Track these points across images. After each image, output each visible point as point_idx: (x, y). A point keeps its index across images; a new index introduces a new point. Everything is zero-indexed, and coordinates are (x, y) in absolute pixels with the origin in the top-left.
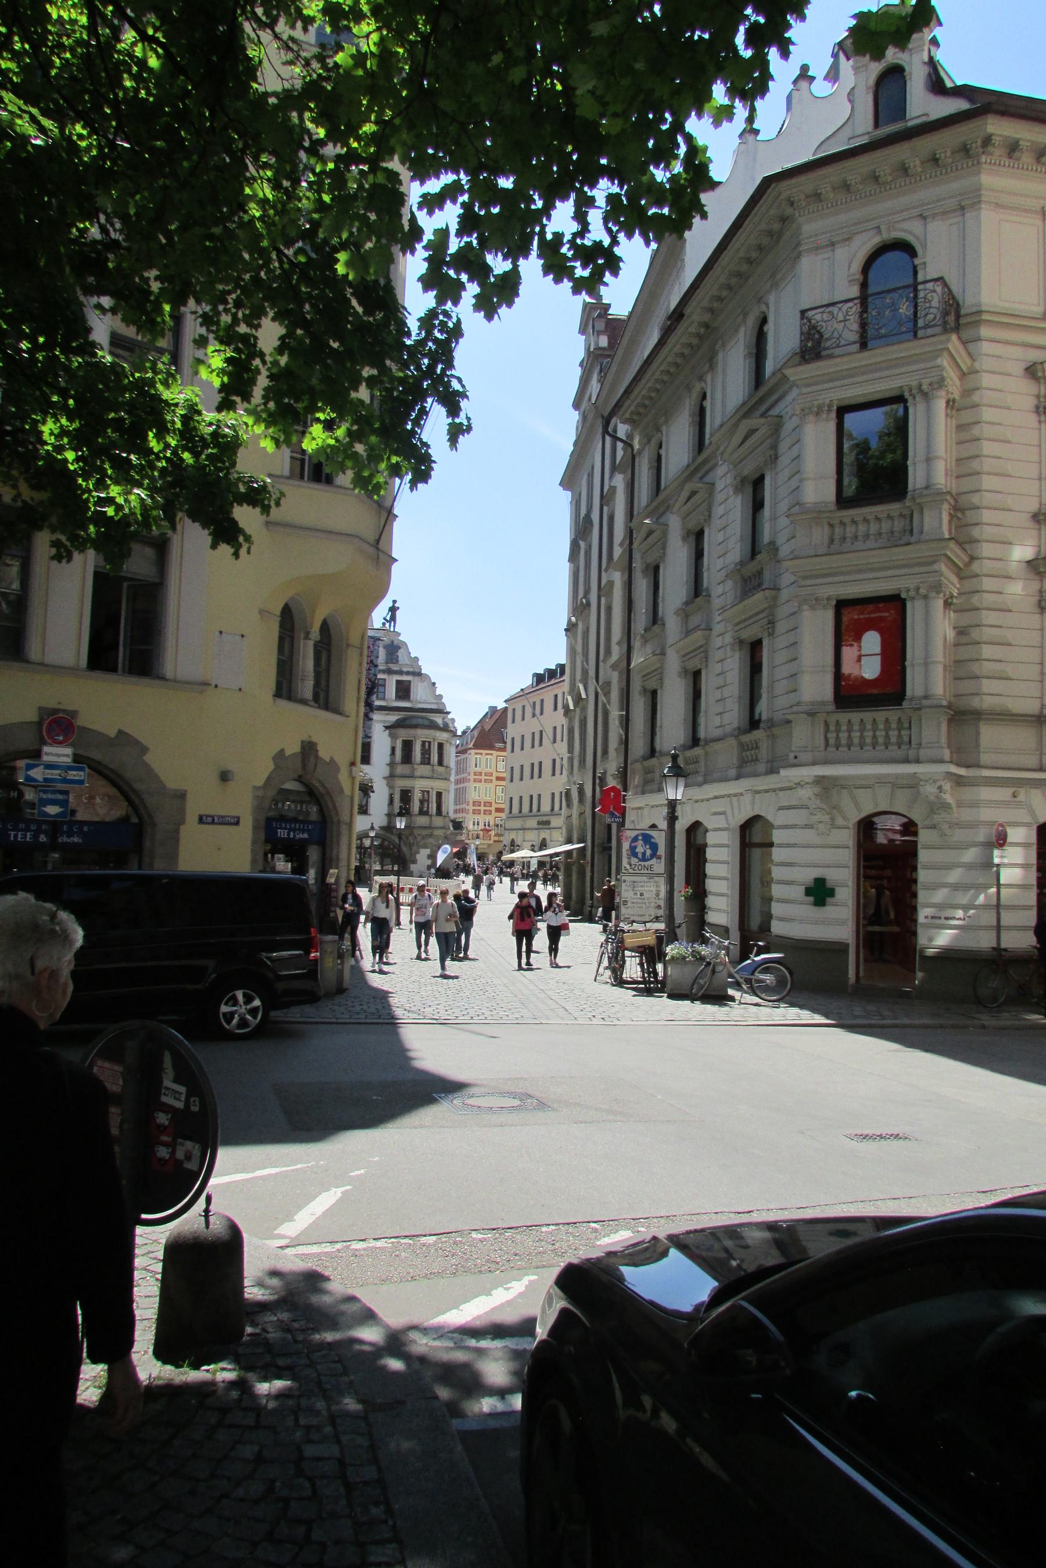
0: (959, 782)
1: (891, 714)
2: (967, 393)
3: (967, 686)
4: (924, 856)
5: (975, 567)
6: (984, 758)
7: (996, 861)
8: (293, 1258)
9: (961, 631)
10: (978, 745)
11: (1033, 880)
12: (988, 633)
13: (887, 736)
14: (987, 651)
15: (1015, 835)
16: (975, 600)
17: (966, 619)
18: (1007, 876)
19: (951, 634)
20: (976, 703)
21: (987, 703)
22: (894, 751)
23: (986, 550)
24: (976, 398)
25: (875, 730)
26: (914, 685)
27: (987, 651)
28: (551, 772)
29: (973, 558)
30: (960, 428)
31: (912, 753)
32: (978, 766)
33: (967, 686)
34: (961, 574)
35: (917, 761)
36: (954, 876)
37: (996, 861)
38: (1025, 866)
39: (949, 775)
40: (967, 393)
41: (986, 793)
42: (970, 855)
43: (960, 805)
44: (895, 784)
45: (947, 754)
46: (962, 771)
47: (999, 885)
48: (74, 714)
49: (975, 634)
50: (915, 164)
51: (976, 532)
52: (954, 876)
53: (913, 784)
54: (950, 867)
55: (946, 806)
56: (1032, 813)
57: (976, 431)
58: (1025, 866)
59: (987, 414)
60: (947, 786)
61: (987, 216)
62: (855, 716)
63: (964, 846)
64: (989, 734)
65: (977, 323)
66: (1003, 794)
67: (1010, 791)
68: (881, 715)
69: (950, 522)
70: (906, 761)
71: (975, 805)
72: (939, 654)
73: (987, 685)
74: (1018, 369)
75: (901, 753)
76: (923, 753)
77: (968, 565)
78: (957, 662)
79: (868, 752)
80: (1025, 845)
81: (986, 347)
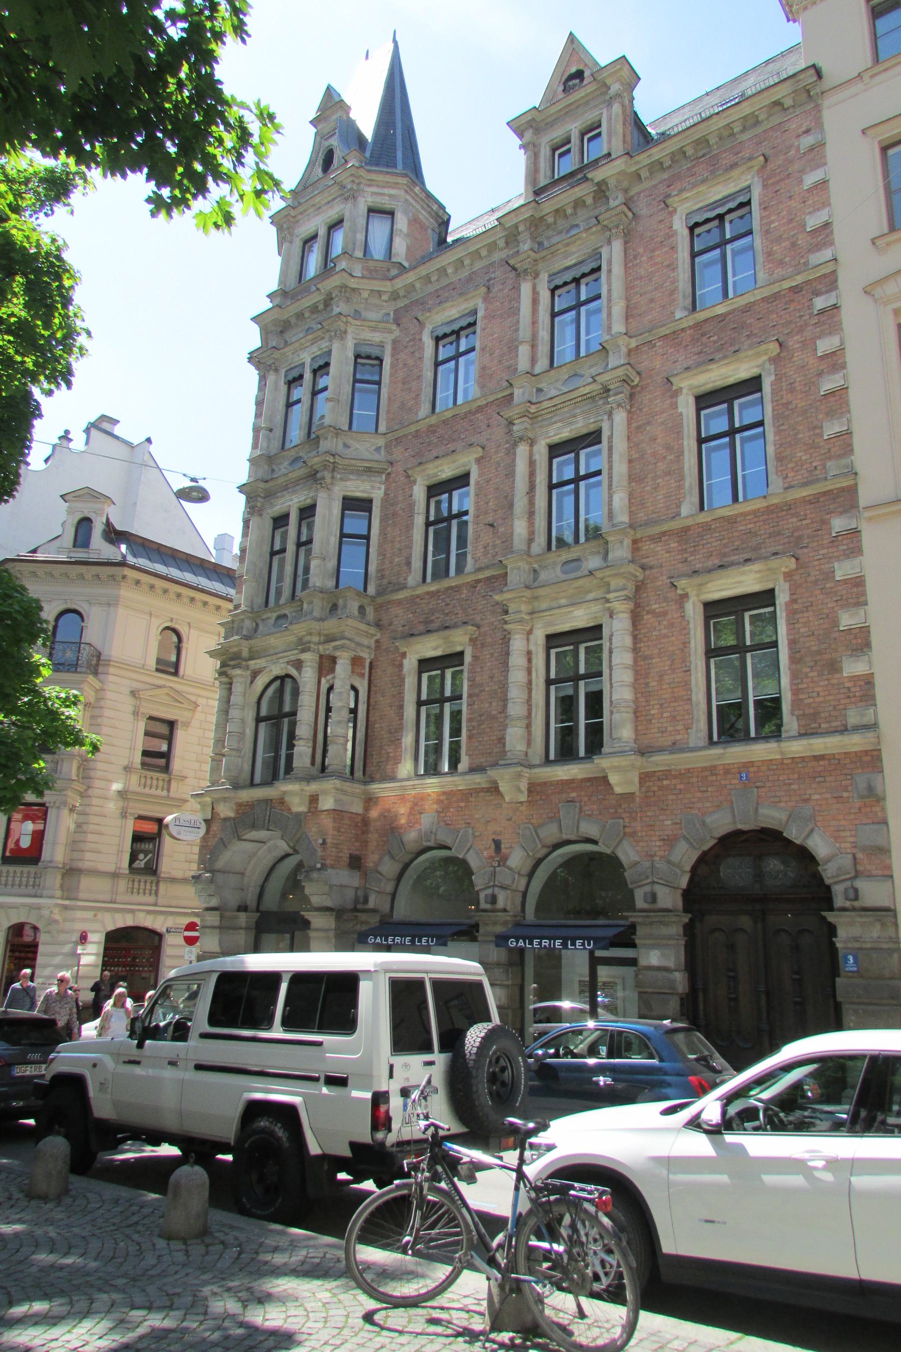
0: (66, 907)
1: (32, 869)
2: (99, 699)
3: (76, 855)
4: (41, 949)
5: (90, 792)
6: (81, 895)
7: (79, 951)
8: (643, 790)
9: (79, 825)
10: (78, 888)
11: (100, 963)
12: (92, 827)
13: (28, 881)
14: (90, 837)
15: (92, 937)
16: (88, 810)
17: (82, 819)
18: (85, 960)
19: (72, 827)
20: (80, 865)
21: (86, 865)
22: (30, 890)
23: (97, 783)
24: (102, 703)
25: (21, 877)
26: (46, 855)
27: (90, 837)
28: (156, 714)
29: (89, 787)
30: (92, 717)
31: (39, 892)
32: (76, 899)
33: (76, 855)
34: (82, 795)
35: (41, 897)
36: (57, 960)
37: (79, 951)
38: (97, 954)
39: (57, 905)
40: (99, 699)
41: (80, 914)
42: (67, 948)
43: (64, 921)
44: (31, 907)
45: (59, 893)
46: (67, 902)
47: (79, 965)
48: (41, 416)
49: (85, 827)
50: (88, 576)
51: (92, 774)
52: (57, 960)
53: (39, 908)
54: (57, 954)
55: (56, 921)
56: (104, 926)
57: (100, 720)
58: (97, 954)
59: (107, 713)
60: (56, 911)
61: (121, 611)
62: (12, 869)
63: (64, 943)
64: (85, 882)
65: (109, 665)
66: (90, 914)
67: (92, 913)
68: (26, 869)
69: (79, 768)
70: (36, 896)
71: (73, 920)
72: (62, 837)
73: (88, 856)
74: (127, 691)
75: (33, 891)
76: (45, 893)
77: (86, 790)
78: (74, 842)
79: (16, 890)
80: (99, 943)
81: (111, 678)
